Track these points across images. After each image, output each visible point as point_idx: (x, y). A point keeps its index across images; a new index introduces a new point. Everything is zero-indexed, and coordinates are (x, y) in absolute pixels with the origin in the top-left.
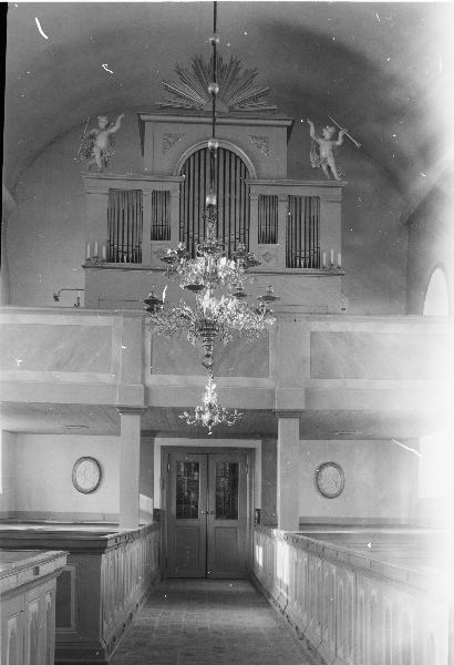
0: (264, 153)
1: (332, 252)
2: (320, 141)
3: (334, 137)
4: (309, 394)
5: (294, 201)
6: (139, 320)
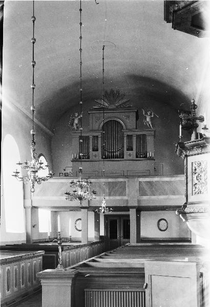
0: (128, 121)
3: (151, 114)
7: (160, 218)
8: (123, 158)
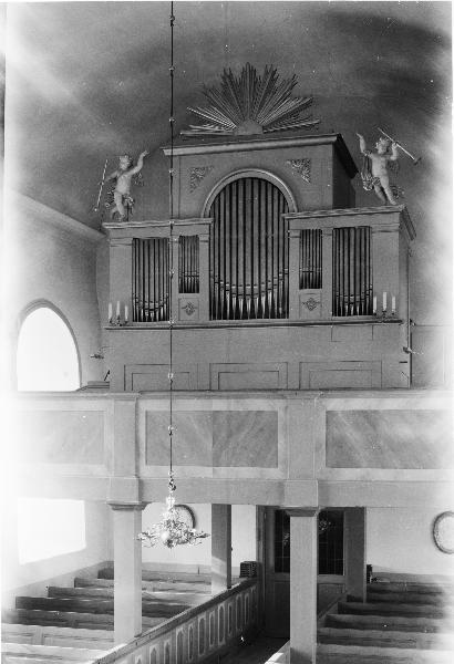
1: (385, 296)
2: (371, 156)
4: (324, 487)
5: (341, 233)
6: (132, 404)
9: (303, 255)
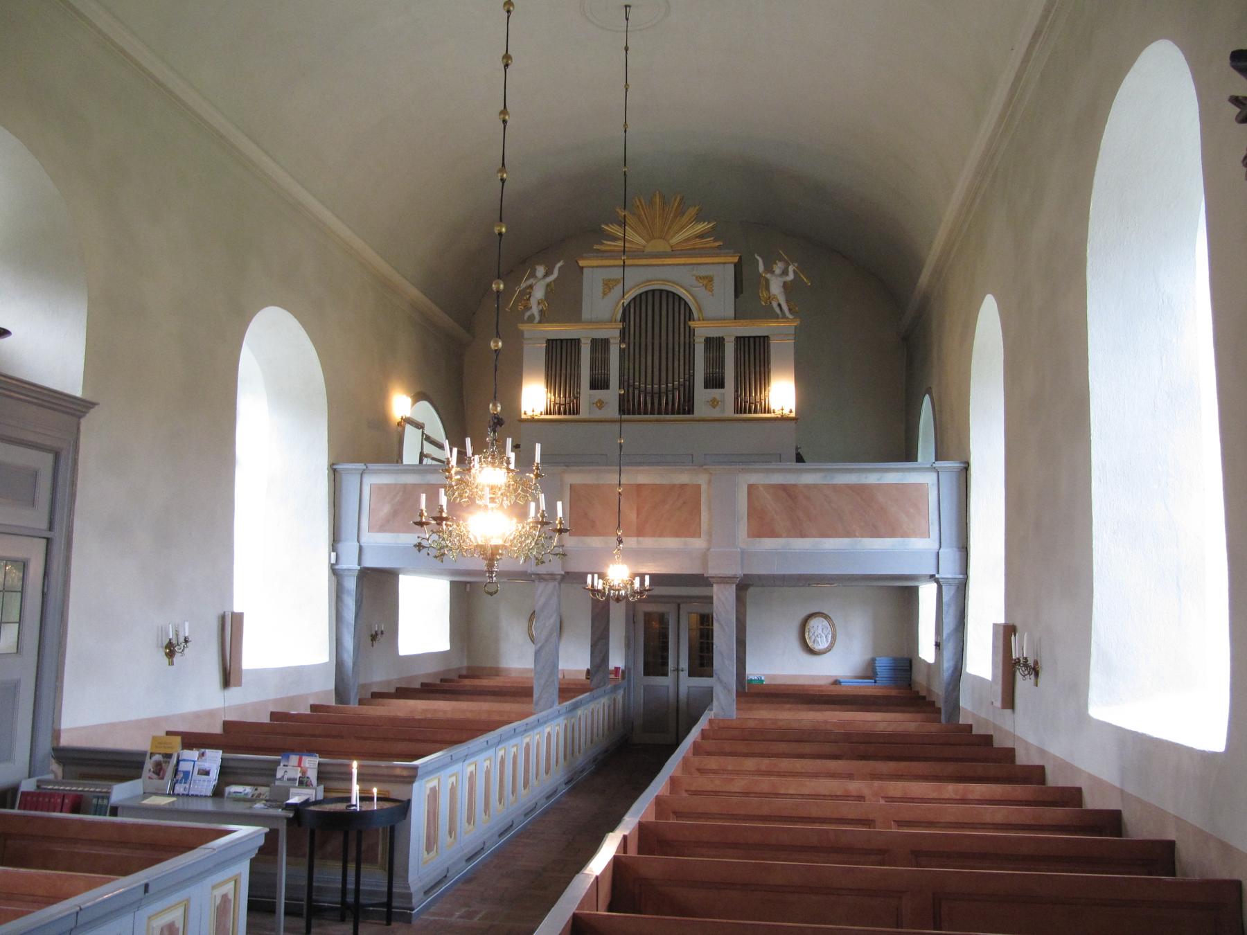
3: (785, 273)
7: (808, 612)
8: (691, 411)
9: (706, 360)
